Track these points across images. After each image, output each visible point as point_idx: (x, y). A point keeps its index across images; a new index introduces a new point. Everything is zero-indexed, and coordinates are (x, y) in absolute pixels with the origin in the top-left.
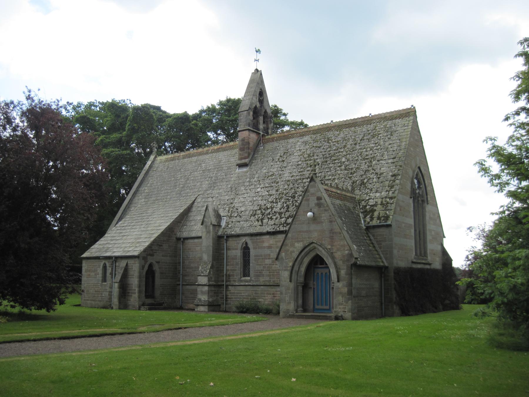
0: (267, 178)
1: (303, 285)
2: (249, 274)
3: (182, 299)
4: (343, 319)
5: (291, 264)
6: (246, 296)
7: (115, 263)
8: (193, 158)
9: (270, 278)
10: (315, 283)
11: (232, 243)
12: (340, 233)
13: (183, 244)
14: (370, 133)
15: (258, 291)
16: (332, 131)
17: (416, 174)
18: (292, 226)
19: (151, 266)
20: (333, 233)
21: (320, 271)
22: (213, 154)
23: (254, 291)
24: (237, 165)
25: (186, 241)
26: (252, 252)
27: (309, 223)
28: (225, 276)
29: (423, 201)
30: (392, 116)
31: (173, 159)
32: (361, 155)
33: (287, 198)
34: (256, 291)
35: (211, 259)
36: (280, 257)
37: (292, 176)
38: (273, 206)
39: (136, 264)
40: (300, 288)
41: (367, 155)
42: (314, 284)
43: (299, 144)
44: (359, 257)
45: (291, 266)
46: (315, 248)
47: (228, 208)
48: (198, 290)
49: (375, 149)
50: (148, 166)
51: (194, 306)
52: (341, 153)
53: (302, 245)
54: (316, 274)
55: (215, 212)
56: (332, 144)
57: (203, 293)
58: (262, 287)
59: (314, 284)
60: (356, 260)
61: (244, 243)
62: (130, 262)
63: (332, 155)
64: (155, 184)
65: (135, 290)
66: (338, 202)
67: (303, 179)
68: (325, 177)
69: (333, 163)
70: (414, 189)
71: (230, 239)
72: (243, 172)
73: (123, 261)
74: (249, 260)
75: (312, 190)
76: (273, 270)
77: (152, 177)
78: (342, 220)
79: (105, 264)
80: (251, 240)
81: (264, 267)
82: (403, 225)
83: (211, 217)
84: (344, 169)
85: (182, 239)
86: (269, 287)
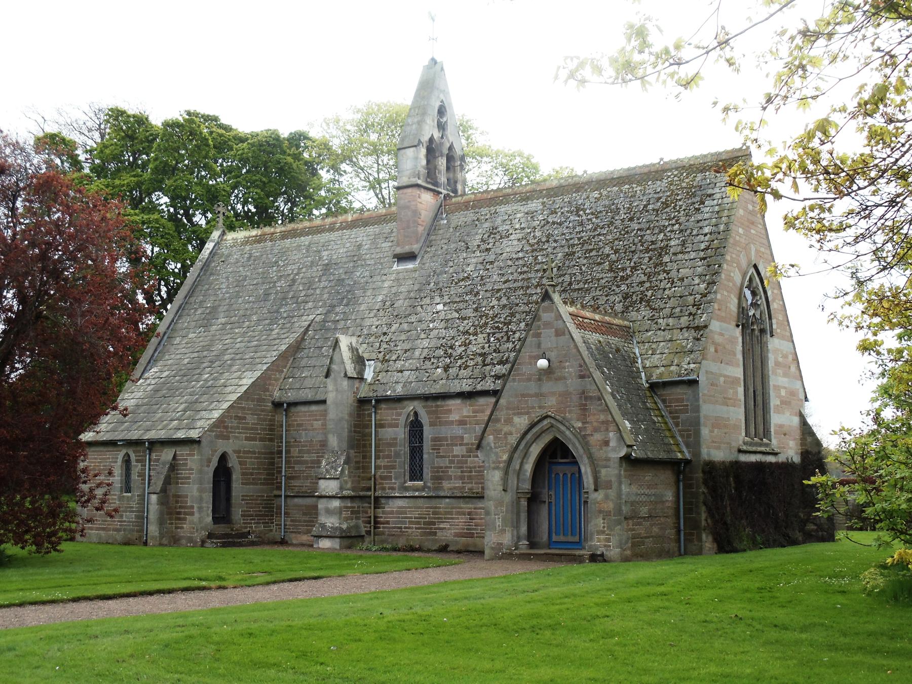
0: (456, 283)
1: (529, 496)
2: (422, 475)
3: (285, 525)
4: (605, 561)
5: (505, 457)
6: (415, 518)
7: (150, 455)
8: (302, 238)
9: (463, 483)
10: (552, 493)
11: (386, 413)
12: (599, 399)
13: (286, 415)
14: (660, 198)
15: (440, 508)
16: (586, 190)
17: (748, 278)
18: (508, 384)
19: (223, 458)
20: (586, 398)
21: (562, 469)
22: (345, 231)
23: (431, 508)
24: (395, 256)
25: (293, 409)
26: (428, 432)
27: (540, 380)
28: (373, 479)
29: (762, 331)
30: (705, 163)
31: (259, 240)
32: (640, 241)
33: (496, 325)
34: (436, 508)
35: (345, 445)
36: (484, 443)
37: (505, 282)
38: (467, 341)
39: (193, 455)
40: (524, 503)
41: (653, 243)
42: (550, 496)
43: (519, 215)
44: (634, 443)
45: (505, 462)
46: (552, 426)
47: (378, 344)
48: (320, 506)
49: (668, 230)
50: (208, 252)
51: (312, 538)
52: (602, 238)
53: (527, 422)
54: (553, 476)
55: (353, 352)
56: (584, 217)
57: (329, 512)
58: (447, 500)
59: (550, 496)
60: (630, 450)
61: (412, 413)
62: (182, 451)
63: (585, 240)
64: (224, 290)
65: (192, 507)
66: (594, 337)
67: (528, 287)
68: (570, 284)
69: (586, 258)
70: (743, 308)
71: (383, 406)
72: (407, 271)
73: (165, 450)
74: (421, 448)
75: (546, 316)
76: (470, 468)
77: (218, 275)
78: (603, 373)
79: (127, 455)
80: (424, 407)
81: (451, 462)
82: (722, 379)
83: (345, 361)
84: (609, 270)
85: (285, 405)
86: (462, 500)
